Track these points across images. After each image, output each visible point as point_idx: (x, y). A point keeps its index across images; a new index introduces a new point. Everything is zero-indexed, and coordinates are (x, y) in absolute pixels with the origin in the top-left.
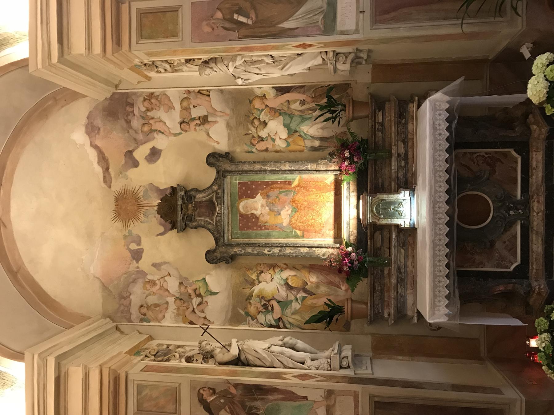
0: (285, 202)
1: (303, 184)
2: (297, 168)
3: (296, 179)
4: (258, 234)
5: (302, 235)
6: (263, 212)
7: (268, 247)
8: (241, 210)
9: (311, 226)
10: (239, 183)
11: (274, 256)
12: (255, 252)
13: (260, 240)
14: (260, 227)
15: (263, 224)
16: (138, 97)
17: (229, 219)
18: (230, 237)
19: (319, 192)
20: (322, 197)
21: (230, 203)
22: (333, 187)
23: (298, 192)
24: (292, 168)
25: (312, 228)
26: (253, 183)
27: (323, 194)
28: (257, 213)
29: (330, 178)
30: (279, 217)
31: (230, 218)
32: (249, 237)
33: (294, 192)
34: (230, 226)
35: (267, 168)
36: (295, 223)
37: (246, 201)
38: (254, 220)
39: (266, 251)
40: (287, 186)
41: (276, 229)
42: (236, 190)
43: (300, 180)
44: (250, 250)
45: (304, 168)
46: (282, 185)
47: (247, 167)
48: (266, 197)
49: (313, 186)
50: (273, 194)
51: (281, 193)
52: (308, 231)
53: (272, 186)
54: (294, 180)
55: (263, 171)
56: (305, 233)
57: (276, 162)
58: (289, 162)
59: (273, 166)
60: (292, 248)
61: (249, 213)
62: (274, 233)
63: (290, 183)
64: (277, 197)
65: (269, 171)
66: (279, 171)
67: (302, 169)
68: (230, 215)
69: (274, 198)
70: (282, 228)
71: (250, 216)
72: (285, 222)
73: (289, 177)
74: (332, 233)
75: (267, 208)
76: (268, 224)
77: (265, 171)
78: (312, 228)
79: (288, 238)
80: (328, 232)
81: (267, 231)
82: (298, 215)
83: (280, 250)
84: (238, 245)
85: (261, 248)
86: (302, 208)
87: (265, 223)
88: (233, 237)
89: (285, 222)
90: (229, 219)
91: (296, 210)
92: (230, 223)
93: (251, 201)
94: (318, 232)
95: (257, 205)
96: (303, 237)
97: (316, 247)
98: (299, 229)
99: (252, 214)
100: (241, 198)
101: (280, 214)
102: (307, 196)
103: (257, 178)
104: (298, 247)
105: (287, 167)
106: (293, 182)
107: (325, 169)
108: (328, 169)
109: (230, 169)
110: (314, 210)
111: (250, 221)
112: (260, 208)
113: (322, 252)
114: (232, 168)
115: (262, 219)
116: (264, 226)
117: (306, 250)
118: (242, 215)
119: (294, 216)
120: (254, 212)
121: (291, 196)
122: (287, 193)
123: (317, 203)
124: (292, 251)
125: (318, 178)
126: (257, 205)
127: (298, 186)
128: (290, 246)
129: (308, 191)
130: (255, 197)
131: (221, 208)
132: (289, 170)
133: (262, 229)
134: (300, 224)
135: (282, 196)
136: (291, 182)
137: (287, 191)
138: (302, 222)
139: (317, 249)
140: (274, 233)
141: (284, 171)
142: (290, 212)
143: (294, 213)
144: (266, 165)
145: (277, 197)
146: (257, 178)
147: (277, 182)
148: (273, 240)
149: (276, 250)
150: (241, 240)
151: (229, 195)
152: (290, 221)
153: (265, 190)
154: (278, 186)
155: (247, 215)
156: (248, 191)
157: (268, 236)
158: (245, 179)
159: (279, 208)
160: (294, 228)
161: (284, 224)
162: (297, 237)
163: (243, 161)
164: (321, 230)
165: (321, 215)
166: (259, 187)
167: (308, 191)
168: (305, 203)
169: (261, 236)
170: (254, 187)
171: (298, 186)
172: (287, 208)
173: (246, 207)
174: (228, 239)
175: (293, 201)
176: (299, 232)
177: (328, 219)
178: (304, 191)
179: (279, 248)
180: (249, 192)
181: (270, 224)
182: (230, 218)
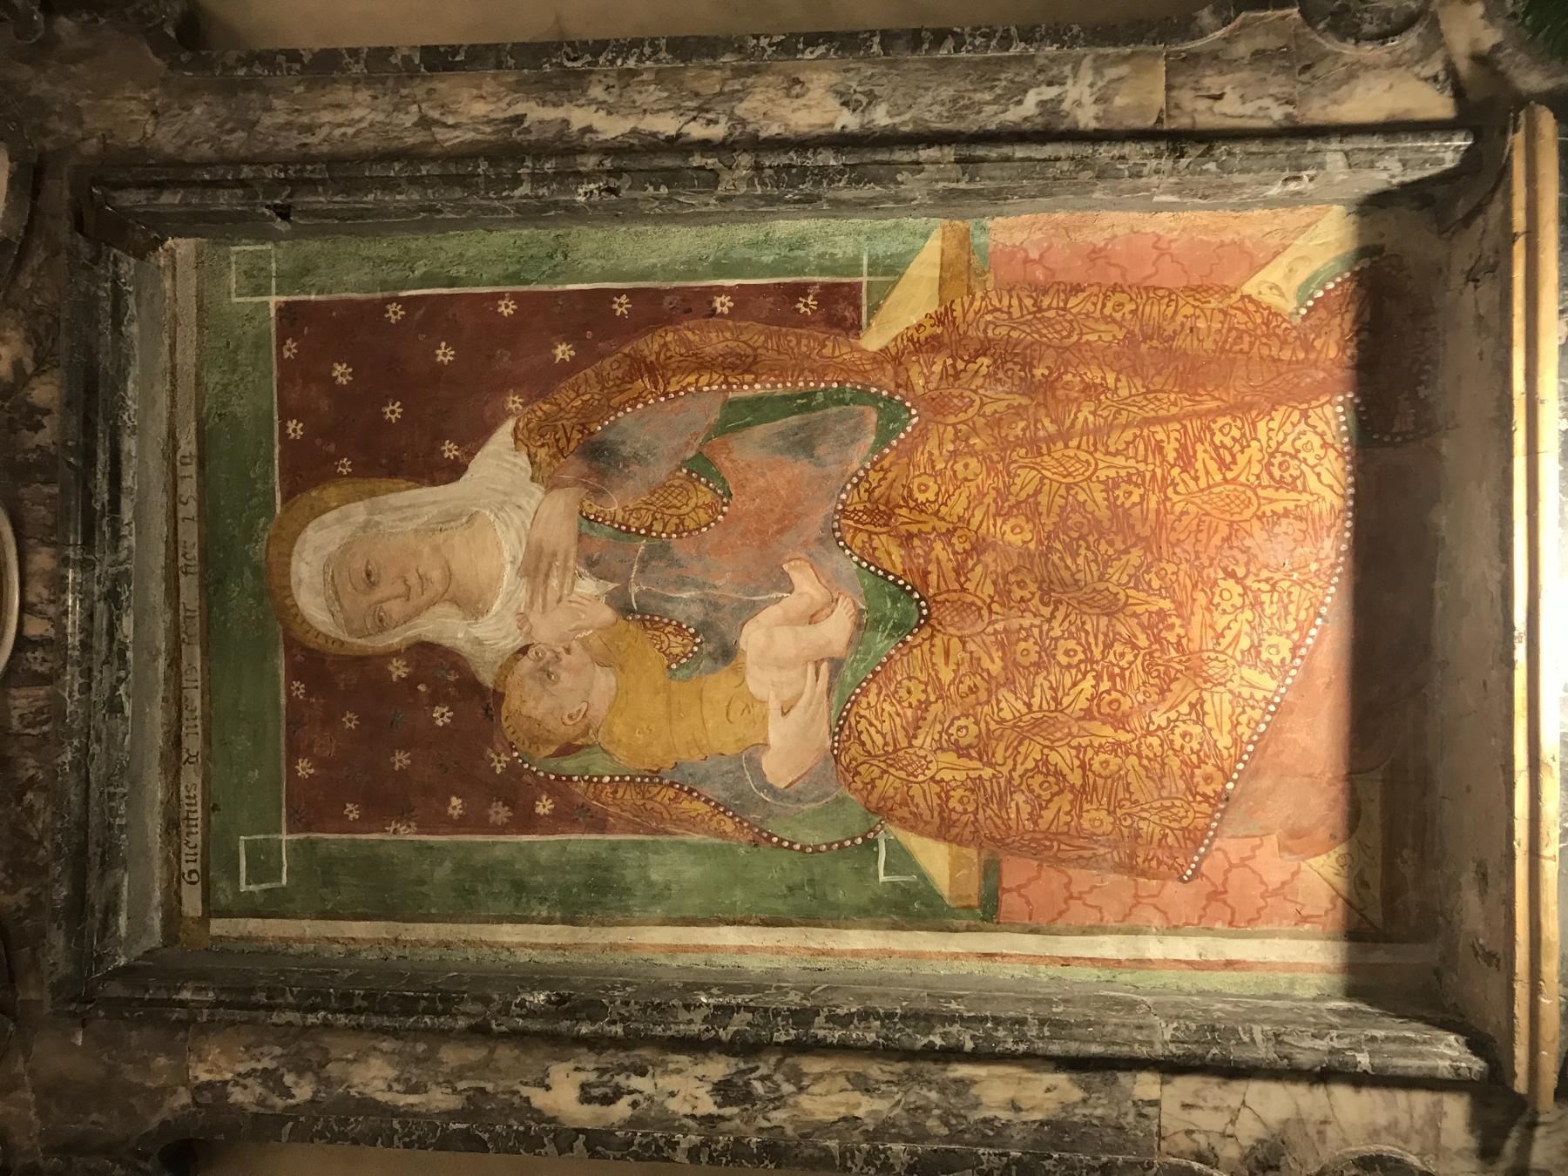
0: (788, 520)
1: (984, 311)
2: (930, 109)
3: (914, 260)
4: (485, 873)
5: (973, 888)
6: (545, 631)
7: (595, 1043)
8: (313, 606)
9: (1083, 793)
10: (290, 315)
11: (658, 1152)
12: (439, 1099)
13: (508, 933)
14: (515, 797)
15: (541, 762)
16: (717, 607)
17: (177, 702)
18: (192, 902)
19: (1173, 402)
20: (1202, 454)
21: (190, 535)
22: (1333, 348)
23: (937, 406)
24: (881, 117)
25: (1095, 817)
26: (433, 316)
27: (1226, 431)
28: (483, 637)
29: (1295, 246)
30: (719, 685)
31: (195, 698)
32: (388, 896)
33: (892, 413)
34: (192, 779)
35: (579, 117)
36: (891, 757)
37: (359, 511)
38: (442, 716)
39: (561, 1093)
40: (804, 342)
41: (692, 823)
42: (258, 393)
43: (958, 272)
44: (373, 1077)
45: (1028, 108)
46: (754, 336)
47: (354, 116)
48: (574, 467)
49: (1102, 335)
50: (660, 427)
51: (739, 416)
52: (1047, 848)
53: (649, 346)
54: (891, 269)
55: (541, 150)
56: (1019, 853)
57: (690, 48)
58: (847, 42)
59: (653, 94)
60: (875, 1070)
61: (395, 639)
62: (672, 866)
63: (841, 307)
64: (701, 467)
65: (610, 149)
66: (724, 148)
67: (991, 117)
68: (193, 656)
69: (660, 471)
70: (744, 801)
71: (398, 669)
72: (788, 745)
73: (832, 239)
74: (1322, 873)
75: (588, 586)
76: (598, 765)
77: (565, 149)
78: (1095, 817)
79: (810, 920)
80: (1272, 865)
81: (581, 841)
82: (938, 662)
83: (725, 1090)
84: (255, 994)
85: (505, 1054)
86: (981, 585)
87: (568, 749)
88: (224, 897)
89: (788, 745)
90: (177, 702)
91: (904, 608)
92: (193, 744)
93: (426, 501)
94: (1163, 850)
95: (482, 555)
96: (988, 911)
97: (1170, 1068)
98: (944, 829)
99: (426, 653)
100: (308, 472)
101: (727, 654)
102: (1035, 446)
103: (480, 257)
104: (952, 1054)
105: (814, 105)
106: (881, 293)
107: (1277, 114)
108: (1318, 111)
109: (166, 138)
110: (1113, 608)
111: (413, 731)
112: (509, 589)
113: (1248, 1130)
114: (189, 125)
115: (530, 704)
116: (558, 787)
117: (1045, 1094)
118: (316, 665)
119: (880, 672)
120: (446, 627)
121: (858, 456)
122: (804, 417)
123: (1155, 540)
124: (867, 1107)
125: (1160, 249)
126: (482, 555)
127: (933, 345)
128: (844, 1049)
129: (1043, 391)
130: (456, 470)
131: (58, 584)
132: (842, 142)
133: (526, 822)
134: (950, 769)
135: (749, 453)
136: (850, 294)
137: (805, 402)
138: (980, 750)
139: (1185, 1086)
140: (672, 866)
141: (780, 144)
142: (837, 629)
143: (881, 643)
144: (570, 85)
145: (701, 467)
146: (480, 257)
147: (696, 304)
148: (654, 942)
149: (687, 1089)
150: (311, 928)
151: (187, 445)
152: (842, 726)
153: (565, 395)
154: (716, 342)
155: (369, 665)
156: (388, 406)
157: (596, 894)
158: (350, 273)
159: (725, 585)
160: (882, 811)
161: (779, 768)
162: (914, 907)
163: (309, 42)
164: (1194, 838)
165: (1195, 670)
166: (504, 359)
167: (1043, 391)
168: (1015, 535)
169: (519, 895)
170: (444, 354)
171: (940, 337)
172: (806, 585)
173: (357, 577)
174: (172, 913)
175: (880, 513)
176: (936, 860)
177: (1280, 710)
178: (1000, 398)
179: (719, 1068)
180: (393, 411)
181: (623, 759)
182: (195, 698)
